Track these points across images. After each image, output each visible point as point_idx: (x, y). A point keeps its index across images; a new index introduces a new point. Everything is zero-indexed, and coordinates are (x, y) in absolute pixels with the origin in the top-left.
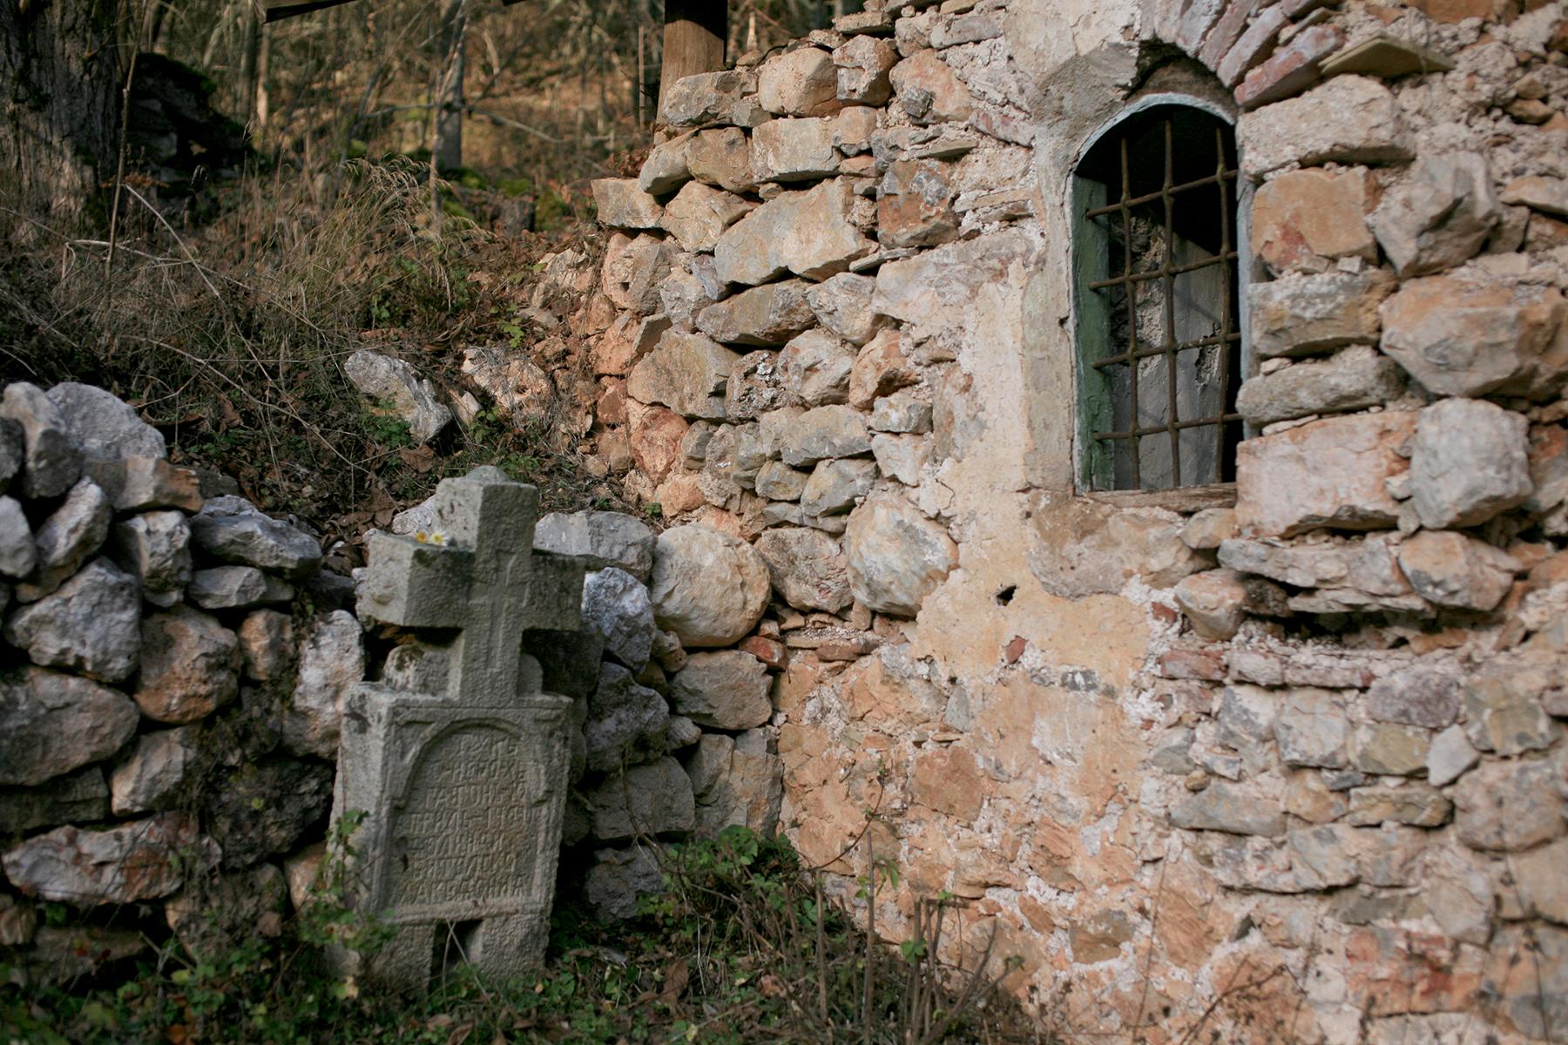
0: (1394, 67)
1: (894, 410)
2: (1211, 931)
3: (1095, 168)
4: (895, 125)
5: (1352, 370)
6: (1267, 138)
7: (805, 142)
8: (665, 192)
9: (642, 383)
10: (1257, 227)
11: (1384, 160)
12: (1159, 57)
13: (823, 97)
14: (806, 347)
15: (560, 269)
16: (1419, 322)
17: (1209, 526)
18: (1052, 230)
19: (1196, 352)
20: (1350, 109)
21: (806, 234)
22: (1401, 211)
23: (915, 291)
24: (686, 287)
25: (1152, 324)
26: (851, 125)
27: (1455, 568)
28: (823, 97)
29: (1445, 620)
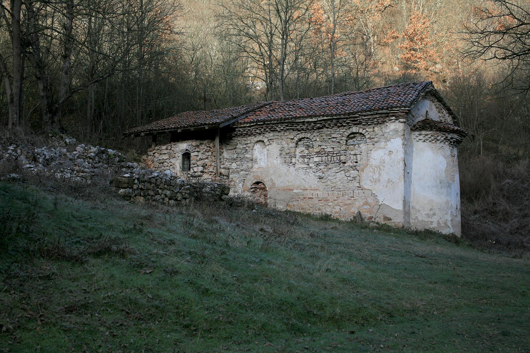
0: (198, 152)
1: (171, 167)
2: (43, 257)
3: (183, 155)
4: (171, 151)
5: (196, 165)
6: (192, 154)
7: (166, 152)
8: (154, 154)
9: (152, 165)
10: (191, 159)
11: (197, 156)
12: (187, 150)
13: (167, 149)
14: (165, 163)
15: (144, 157)
16: (199, 163)
17: (189, 172)
18: (181, 158)
19: (336, 19)
20: (196, 153)
21: (165, 157)
22: (198, 158)
23: (173, 161)
24: (155, 159)
25: (186, 163)
26: (168, 151)
27: (199, 173)
28: (167, 149)
29: (200, 176)
